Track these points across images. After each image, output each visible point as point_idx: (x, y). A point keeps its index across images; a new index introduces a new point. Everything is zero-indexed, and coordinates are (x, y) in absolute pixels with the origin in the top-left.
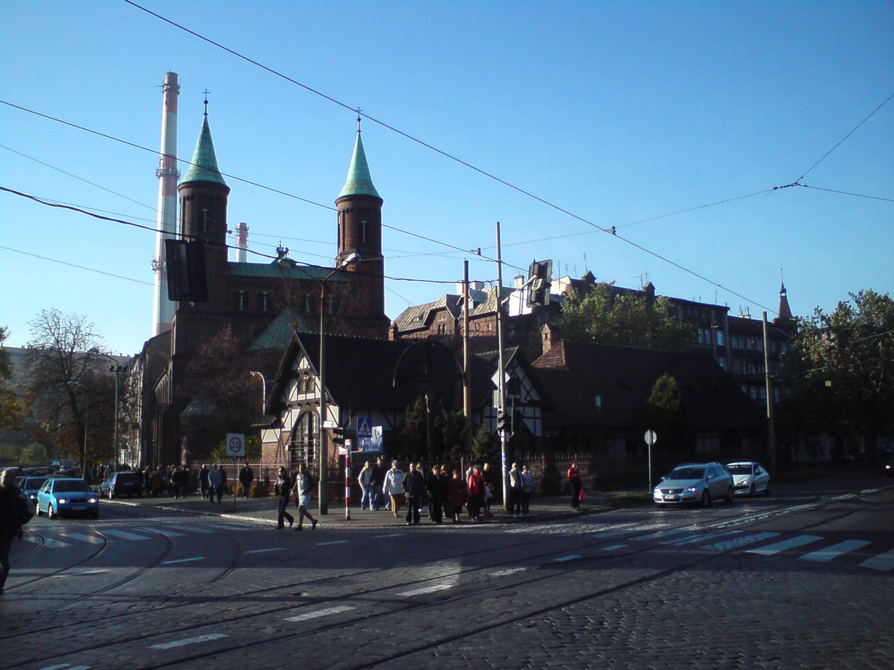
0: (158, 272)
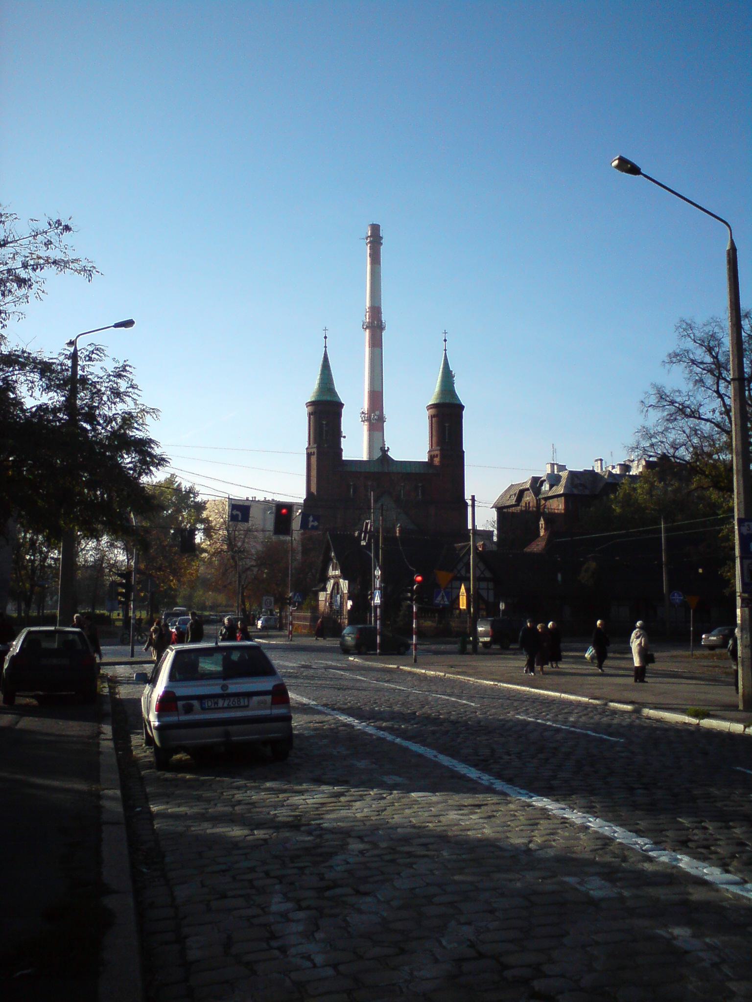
0: (366, 423)
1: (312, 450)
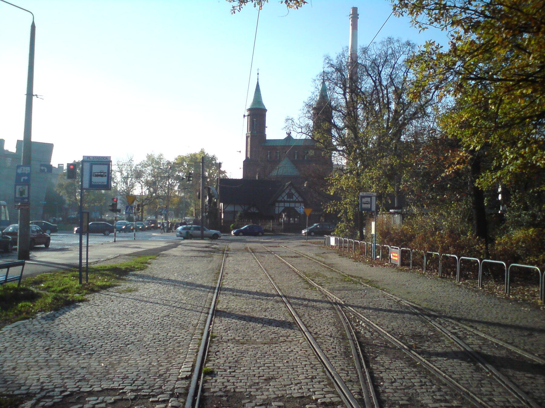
1: (248, 135)
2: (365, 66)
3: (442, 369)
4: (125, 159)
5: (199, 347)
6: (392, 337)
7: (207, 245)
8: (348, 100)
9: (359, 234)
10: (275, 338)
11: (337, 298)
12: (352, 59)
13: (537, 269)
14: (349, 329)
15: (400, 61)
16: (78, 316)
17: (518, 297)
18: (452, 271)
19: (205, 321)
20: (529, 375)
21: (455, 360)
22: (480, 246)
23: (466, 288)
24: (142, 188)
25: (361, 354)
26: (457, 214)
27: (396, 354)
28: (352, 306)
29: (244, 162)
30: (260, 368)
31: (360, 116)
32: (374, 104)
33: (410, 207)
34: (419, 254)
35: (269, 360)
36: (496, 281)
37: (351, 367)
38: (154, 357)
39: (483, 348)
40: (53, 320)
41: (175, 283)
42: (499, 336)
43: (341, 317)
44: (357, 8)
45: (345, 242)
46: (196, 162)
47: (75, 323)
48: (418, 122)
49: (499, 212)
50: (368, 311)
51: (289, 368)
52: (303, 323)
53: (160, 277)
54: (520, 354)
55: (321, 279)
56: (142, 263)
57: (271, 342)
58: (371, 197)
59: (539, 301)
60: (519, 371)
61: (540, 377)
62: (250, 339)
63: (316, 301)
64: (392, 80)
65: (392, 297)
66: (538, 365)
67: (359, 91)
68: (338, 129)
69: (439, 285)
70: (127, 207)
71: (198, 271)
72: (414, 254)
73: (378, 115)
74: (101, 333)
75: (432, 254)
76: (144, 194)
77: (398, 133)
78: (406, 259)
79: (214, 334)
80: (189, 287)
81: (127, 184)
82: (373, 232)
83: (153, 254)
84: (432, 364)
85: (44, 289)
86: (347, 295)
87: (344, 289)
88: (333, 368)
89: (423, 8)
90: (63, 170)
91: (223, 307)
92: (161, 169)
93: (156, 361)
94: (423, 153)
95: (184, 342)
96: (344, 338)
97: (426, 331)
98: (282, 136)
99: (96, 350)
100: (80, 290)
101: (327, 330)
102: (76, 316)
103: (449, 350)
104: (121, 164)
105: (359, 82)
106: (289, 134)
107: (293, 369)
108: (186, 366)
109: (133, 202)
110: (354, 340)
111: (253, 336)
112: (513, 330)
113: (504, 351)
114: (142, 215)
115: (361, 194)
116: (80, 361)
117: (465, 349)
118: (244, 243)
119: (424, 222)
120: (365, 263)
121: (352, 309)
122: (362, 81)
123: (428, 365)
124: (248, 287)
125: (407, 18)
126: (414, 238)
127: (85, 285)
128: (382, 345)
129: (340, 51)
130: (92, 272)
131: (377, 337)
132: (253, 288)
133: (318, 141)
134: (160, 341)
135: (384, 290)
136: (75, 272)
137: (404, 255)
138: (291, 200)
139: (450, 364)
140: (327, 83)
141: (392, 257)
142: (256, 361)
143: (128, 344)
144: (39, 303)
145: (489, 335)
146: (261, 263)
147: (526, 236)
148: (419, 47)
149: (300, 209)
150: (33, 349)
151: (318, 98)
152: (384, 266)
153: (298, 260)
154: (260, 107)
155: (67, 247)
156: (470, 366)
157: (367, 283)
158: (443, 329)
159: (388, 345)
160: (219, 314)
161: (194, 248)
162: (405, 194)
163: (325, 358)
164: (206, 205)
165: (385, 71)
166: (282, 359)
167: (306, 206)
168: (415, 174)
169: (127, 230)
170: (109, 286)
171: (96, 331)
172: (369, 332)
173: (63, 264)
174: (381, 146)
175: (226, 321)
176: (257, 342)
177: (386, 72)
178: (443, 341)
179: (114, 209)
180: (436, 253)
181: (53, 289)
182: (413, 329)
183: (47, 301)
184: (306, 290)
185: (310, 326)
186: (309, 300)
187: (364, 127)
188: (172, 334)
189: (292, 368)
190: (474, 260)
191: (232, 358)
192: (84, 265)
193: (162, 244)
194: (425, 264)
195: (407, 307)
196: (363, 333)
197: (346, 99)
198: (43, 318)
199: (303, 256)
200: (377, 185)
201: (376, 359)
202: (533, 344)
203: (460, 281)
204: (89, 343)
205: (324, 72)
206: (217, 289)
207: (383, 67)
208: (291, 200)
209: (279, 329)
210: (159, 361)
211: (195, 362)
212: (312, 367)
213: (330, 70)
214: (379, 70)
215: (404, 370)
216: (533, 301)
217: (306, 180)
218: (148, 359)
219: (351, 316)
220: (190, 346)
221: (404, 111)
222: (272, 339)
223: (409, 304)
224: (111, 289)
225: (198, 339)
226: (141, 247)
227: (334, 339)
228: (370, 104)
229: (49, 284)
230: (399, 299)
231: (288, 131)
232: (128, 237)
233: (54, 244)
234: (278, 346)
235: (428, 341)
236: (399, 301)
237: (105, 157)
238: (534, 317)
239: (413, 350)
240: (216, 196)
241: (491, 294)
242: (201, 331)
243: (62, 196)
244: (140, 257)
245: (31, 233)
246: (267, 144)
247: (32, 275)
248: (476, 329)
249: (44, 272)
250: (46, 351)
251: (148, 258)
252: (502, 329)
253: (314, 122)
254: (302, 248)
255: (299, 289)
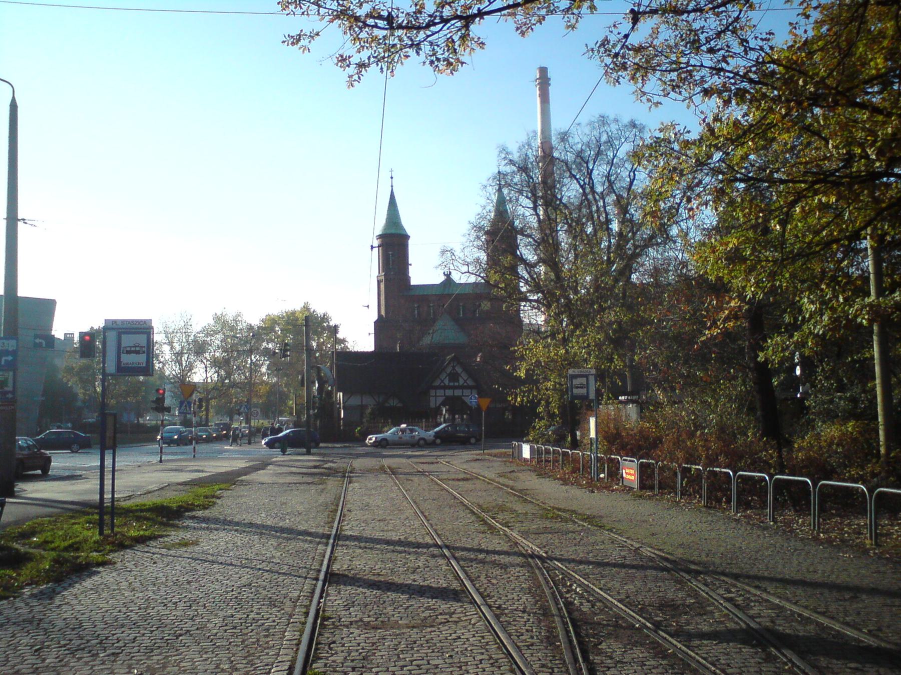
2: (566, 163)
3: (710, 659)
4: (176, 323)
5: (301, 635)
6: (627, 609)
7: (318, 464)
8: (541, 217)
9: (569, 439)
10: (431, 616)
11: (534, 548)
12: (543, 151)
13: (863, 489)
14: (555, 598)
15: (622, 153)
16: (95, 589)
17: (833, 535)
18: (725, 495)
19: (313, 592)
20: (853, 665)
21: (731, 644)
22: (770, 454)
23: (748, 523)
24: (206, 371)
25: (574, 639)
26: (730, 400)
27: (632, 637)
28: (559, 560)
29: (375, 323)
30: (405, 668)
31: (563, 244)
32: (583, 224)
33: (653, 391)
34: (669, 469)
35: (420, 655)
36: (796, 511)
37: (557, 662)
38: (223, 655)
39: (778, 622)
40: (51, 599)
41: (262, 530)
42: (803, 602)
43: (541, 579)
44: (546, 68)
45: (547, 452)
46: (295, 326)
47: (89, 602)
48: (657, 251)
49: (799, 396)
50: (586, 567)
51: (453, 667)
52: (477, 590)
53: (236, 520)
54: (838, 631)
55: (506, 516)
56: (206, 497)
57: (424, 624)
58: (586, 376)
59: (868, 542)
60: (838, 659)
61: (872, 668)
62: (389, 621)
63: (499, 553)
64: (611, 184)
65: (626, 542)
66: (868, 649)
67: (558, 202)
68: (530, 266)
69: (704, 519)
70: (181, 403)
71: (300, 508)
72: (662, 469)
73: (592, 242)
74: (135, 617)
75: (690, 469)
76: (209, 380)
77: (626, 271)
78: (647, 477)
79: (327, 614)
80: (285, 535)
81: (180, 364)
82: (593, 434)
83: (225, 482)
84: (693, 651)
85: (38, 546)
86: (552, 541)
87: (546, 531)
88: (528, 664)
89: (654, 70)
90: (74, 343)
91: (342, 567)
92: (237, 338)
93: (228, 662)
94: (669, 302)
95: (275, 628)
96: (546, 613)
97: (682, 597)
98: (437, 278)
99: (125, 646)
100: (101, 545)
101: (518, 600)
102: (92, 589)
103: (721, 628)
104: (171, 331)
105: (558, 188)
106: (448, 276)
107: (460, 667)
108: (278, 669)
109: (191, 395)
110: (562, 617)
111: (393, 615)
112: (826, 591)
113: (812, 627)
114: (207, 415)
115: (571, 371)
116: (96, 668)
117: (748, 625)
118: (380, 459)
119: (676, 415)
120: (580, 486)
121: (560, 565)
122: (563, 186)
123: (687, 654)
124: (385, 533)
125: (627, 87)
126: (661, 442)
127: (108, 536)
128: (610, 623)
129: (524, 139)
130: (120, 515)
131: (602, 610)
132: (394, 534)
133: (496, 286)
134: (235, 628)
135: (612, 531)
136: (93, 515)
137: (644, 471)
138: (456, 384)
139: (724, 651)
140: (505, 191)
141: (624, 475)
142: (399, 657)
143: (181, 635)
144: (27, 571)
145: (788, 600)
146: (406, 491)
147: (843, 434)
148: (650, 130)
149: (471, 399)
150: (12, 652)
151: (493, 214)
152: (613, 491)
153: (468, 485)
154: (398, 232)
155: (79, 473)
156: (756, 653)
157: (584, 520)
158: (711, 593)
159: (620, 622)
160: (336, 579)
161: (294, 470)
162: (643, 371)
163: (514, 648)
164: (314, 397)
165: (598, 170)
166: (442, 653)
167: (481, 394)
168: (660, 338)
169: (183, 441)
170: (151, 538)
171: (125, 613)
172: (588, 601)
173: (72, 503)
174: (600, 291)
175: (347, 591)
176: (400, 625)
177: (599, 171)
178: (712, 612)
179: (160, 406)
180: (697, 467)
181: (53, 545)
182: (661, 594)
183: (42, 566)
184: (483, 536)
185: (488, 596)
186: (488, 552)
187: (570, 261)
188: (256, 616)
189: (458, 667)
190: (760, 477)
191: (358, 654)
192: (107, 504)
193: (241, 464)
194: (679, 485)
195: (651, 559)
196: (578, 604)
197: (538, 215)
198: (33, 596)
199: (477, 478)
200: (597, 357)
201: (600, 647)
202: (859, 613)
203: (737, 512)
204: (114, 635)
205: (499, 172)
206: (332, 537)
207: (594, 163)
208: (456, 384)
209: (436, 602)
210: (232, 662)
211: (293, 661)
212: (492, 664)
213: (509, 169)
214: (588, 168)
215: (647, 663)
216: (858, 541)
217: (480, 351)
218: (214, 659)
219: (558, 576)
220: (286, 634)
221: (634, 234)
222: (426, 618)
223: (654, 554)
224: (153, 543)
225: (300, 622)
226: (206, 469)
227: (529, 616)
228: (577, 224)
229: (47, 537)
230: (637, 545)
231: (446, 270)
232: (183, 453)
233: (58, 468)
234: (435, 631)
235: (686, 613)
236: (638, 548)
237: (142, 321)
238: (860, 568)
239: (663, 631)
240: (331, 381)
241: (789, 531)
242: (304, 610)
243: (71, 387)
244: (202, 487)
245: (17, 450)
246: (412, 293)
247: (17, 523)
248: (765, 590)
249: (38, 517)
250: (36, 654)
251: (216, 487)
252: (809, 590)
253: (488, 255)
254: (476, 464)
255: (470, 533)
